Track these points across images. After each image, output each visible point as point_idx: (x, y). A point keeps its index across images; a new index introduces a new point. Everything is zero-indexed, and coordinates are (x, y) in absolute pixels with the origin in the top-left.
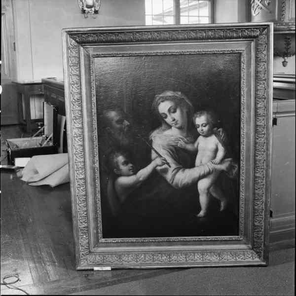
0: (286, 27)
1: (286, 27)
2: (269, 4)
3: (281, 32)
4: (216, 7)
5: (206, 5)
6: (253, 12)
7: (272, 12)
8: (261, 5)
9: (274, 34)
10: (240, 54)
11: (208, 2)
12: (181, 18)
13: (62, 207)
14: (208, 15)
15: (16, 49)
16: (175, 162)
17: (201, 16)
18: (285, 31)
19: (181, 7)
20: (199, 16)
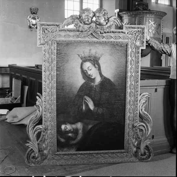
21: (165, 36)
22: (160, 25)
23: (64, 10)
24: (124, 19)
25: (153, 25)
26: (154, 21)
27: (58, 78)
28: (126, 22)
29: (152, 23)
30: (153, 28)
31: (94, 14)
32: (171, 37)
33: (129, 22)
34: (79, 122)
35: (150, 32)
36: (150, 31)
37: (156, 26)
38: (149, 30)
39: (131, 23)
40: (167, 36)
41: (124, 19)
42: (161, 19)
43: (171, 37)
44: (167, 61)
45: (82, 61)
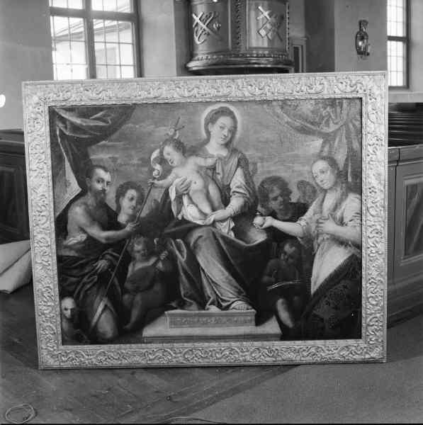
0: (243, 59)
1: (243, 59)
2: (219, 28)
3: (232, 66)
4: (142, 35)
5: (127, 28)
6: (196, 39)
7: (223, 39)
8: (207, 30)
9: (307, 72)
10: (361, 98)
11: (130, 23)
12: (96, 44)
13: (66, 338)
14: (131, 42)
15: (410, 86)
16: (234, 281)
17: (122, 43)
18: (239, 64)
19: (95, 27)
20: (397, 56)
21: (292, 45)
22: (282, 18)
23: (386, 21)
24: (196, 5)
25: (268, 17)
26: (269, 9)
27: (57, 201)
28: (201, 14)
29: (266, 14)
30: (268, 26)
31: (210, 124)
32: (302, 46)
33: (211, 13)
34: (118, 220)
35: (263, 35)
36: (263, 32)
37: (274, 21)
38: (260, 32)
39: (215, 14)
40: (296, 43)
41: (196, 5)
42: (285, 4)
43: (302, 46)
44: (393, 197)
45: (110, 173)
